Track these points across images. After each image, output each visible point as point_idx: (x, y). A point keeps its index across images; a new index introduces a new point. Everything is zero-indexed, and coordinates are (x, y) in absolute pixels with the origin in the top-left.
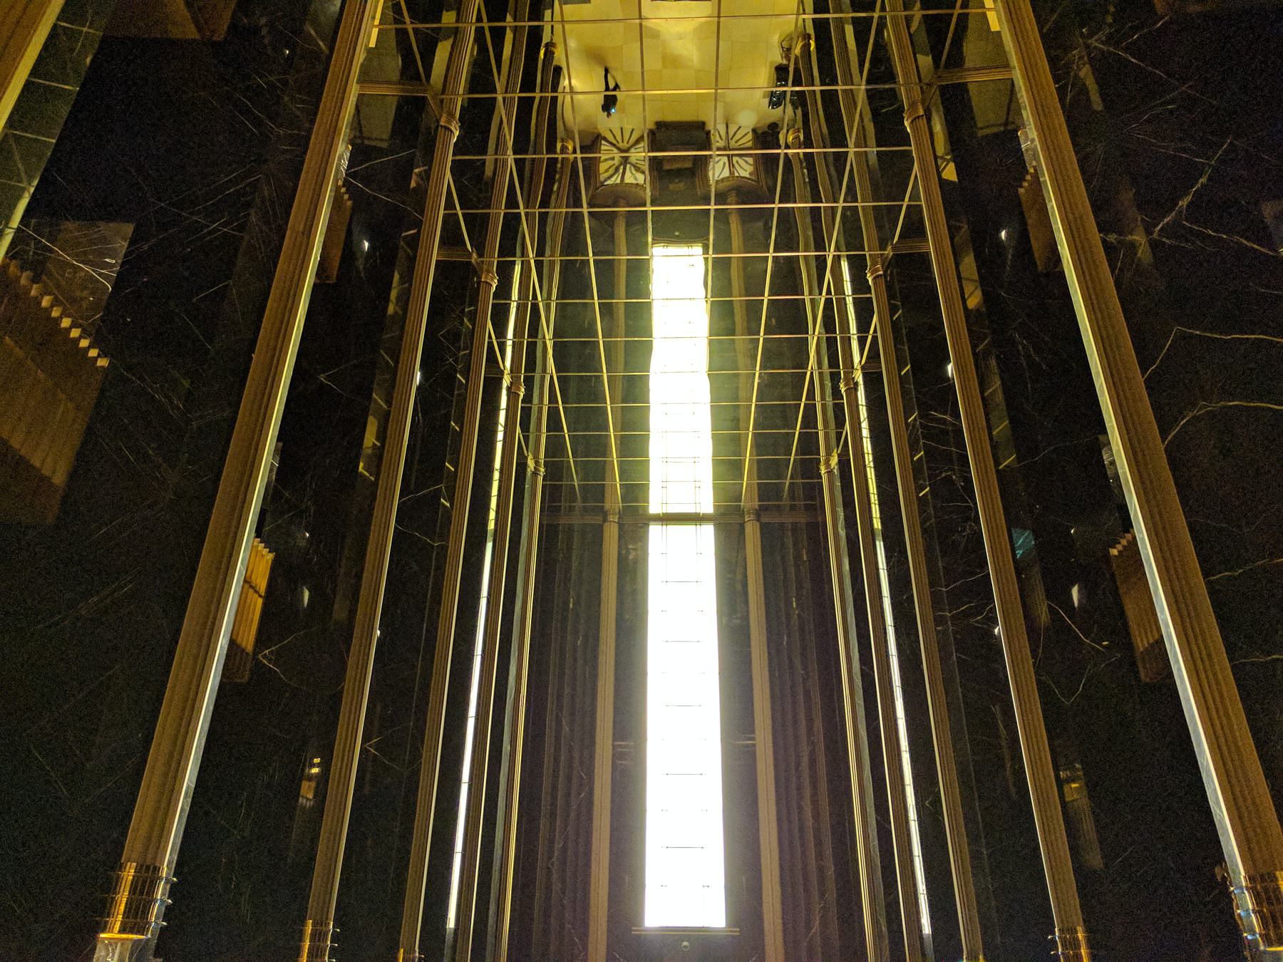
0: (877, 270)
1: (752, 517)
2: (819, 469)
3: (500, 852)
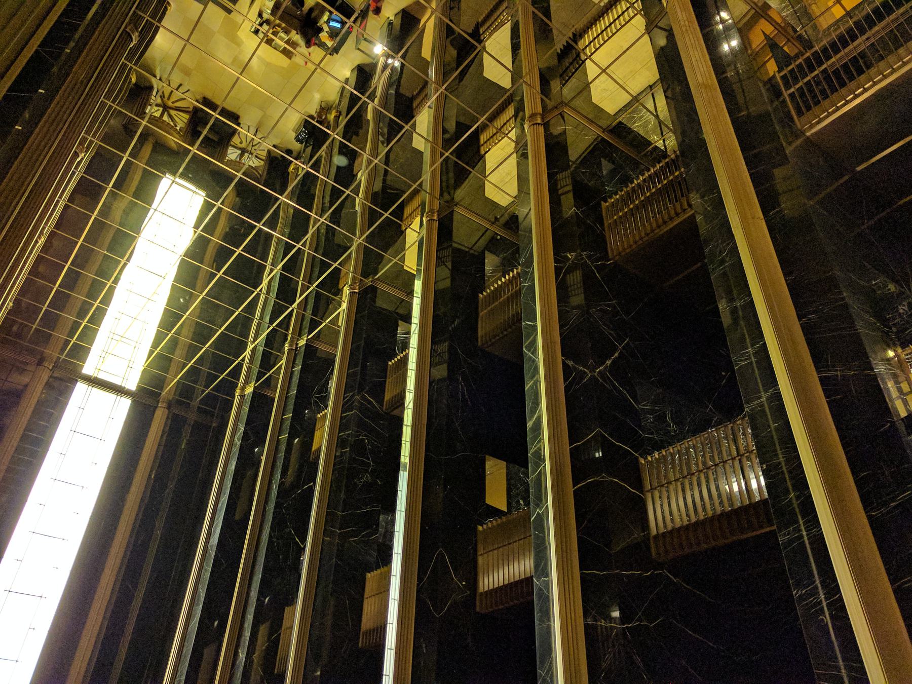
0: (355, 288)
1: (165, 405)
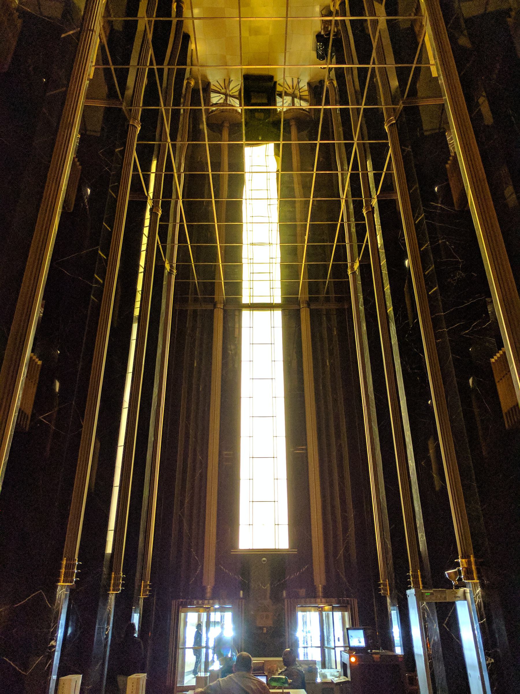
0: (392, 120)
1: (305, 305)
2: (347, 272)
3: (146, 502)
